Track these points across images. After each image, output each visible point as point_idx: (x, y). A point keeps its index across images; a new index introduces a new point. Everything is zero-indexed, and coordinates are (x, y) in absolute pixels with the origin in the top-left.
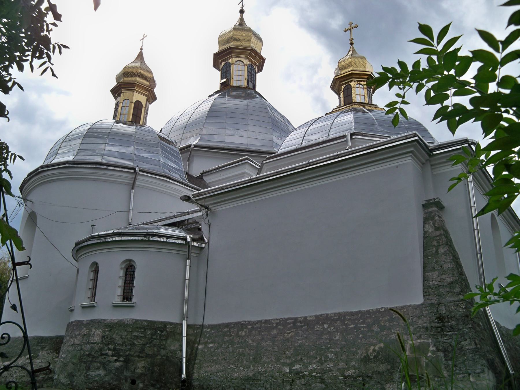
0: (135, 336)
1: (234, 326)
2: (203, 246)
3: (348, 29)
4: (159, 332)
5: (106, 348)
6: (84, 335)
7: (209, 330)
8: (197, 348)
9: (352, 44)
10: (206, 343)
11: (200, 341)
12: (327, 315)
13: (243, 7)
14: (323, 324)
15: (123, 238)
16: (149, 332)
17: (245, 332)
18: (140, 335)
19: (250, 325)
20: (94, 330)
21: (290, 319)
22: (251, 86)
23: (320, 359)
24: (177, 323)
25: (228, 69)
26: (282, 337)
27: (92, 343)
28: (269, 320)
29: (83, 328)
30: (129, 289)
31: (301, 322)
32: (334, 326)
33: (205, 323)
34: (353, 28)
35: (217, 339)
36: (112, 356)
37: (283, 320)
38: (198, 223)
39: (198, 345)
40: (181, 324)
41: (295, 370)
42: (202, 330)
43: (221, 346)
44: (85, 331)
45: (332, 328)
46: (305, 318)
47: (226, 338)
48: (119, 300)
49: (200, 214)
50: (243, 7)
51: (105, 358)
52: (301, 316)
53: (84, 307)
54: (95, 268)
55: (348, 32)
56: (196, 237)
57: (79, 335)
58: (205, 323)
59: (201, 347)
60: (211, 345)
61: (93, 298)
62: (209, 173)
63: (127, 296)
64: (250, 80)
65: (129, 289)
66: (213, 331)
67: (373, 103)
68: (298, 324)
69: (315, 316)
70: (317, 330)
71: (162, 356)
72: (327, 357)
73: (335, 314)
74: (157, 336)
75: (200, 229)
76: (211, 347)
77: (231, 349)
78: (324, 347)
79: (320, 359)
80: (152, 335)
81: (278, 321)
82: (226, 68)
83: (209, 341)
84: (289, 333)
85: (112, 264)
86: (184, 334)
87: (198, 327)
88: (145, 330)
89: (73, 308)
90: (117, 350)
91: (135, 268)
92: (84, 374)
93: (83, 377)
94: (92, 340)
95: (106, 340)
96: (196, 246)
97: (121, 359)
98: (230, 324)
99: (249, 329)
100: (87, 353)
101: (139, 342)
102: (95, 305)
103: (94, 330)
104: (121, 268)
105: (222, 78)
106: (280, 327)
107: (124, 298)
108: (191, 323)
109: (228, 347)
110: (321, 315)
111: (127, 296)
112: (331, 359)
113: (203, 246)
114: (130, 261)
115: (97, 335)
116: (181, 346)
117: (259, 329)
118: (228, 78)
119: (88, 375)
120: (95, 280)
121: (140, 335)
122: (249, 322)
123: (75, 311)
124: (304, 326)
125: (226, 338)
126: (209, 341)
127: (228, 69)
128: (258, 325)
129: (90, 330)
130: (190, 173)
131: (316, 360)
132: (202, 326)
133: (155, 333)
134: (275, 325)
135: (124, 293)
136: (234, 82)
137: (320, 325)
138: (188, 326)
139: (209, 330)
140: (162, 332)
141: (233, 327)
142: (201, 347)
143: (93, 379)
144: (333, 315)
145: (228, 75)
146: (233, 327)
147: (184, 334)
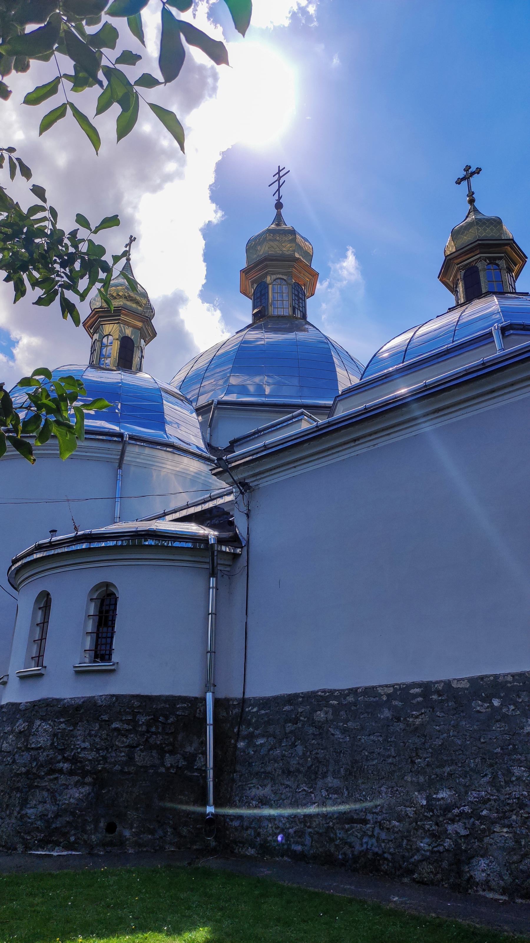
0: (116, 729)
1: (303, 701)
2: (238, 551)
3: (463, 179)
4: (161, 719)
5: (60, 757)
6: (20, 732)
7: (255, 710)
8: (235, 746)
9: (472, 201)
10: (251, 737)
11: (239, 731)
12: (496, 677)
13: (280, 198)
14: (488, 699)
15: (95, 545)
16: (143, 719)
17: (326, 713)
18: (126, 726)
19: (336, 698)
20: (38, 722)
21: (414, 685)
22: (299, 314)
23: (495, 777)
24: (196, 698)
25: (263, 292)
26: (402, 726)
27: (32, 749)
28: (373, 688)
29: (19, 719)
30: (106, 638)
31: (439, 693)
32: (515, 704)
33: (247, 696)
34: (473, 174)
35: (271, 729)
36: (71, 773)
37: (400, 689)
38: (228, 513)
39: (237, 741)
40: (204, 699)
41: (439, 800)
42: (243, 710)
43: (280, 742)
44: (21, 725)
45: (512, 707)
46: (448, 684)
47: (290, 727)
48: (87, 660)
49: (231, 498)
50: (280, 198)
51: (56, 779)
52: (438, 679)
53: (24, 678)
54: (44, 602)
55: (465, 183)
56: (226, 535)
57: (12, 731)
58: (247, 696)
59: (241, 744)
60: (260, 741)
61: (39, 659)
62: (244, 441)
63: (102, 650)
64: (297, 306)
65: (106, 638)
66: (263, 712)
67: (517, 291)
68: (435, 697)
69: (471, 680)
70: (479, 712)
71: (168, 769)
72: (509, 772)
73: (513, 676)
74: (157, 728)
75: (232, 523)
76: (262, 745)
77: (300, 749)
78: (499, 750)
79: (495, 777)
80: (148, 724)
81: (391, 690)
82: (261, 292)
83: (257, 732)
84: (417, 717)
85: (73, 595)
86: (210, 719)
87: (235, 703)
88: (135, 714)
89: (5, 679)
90: (81, 762)
91: (116, 599)
92: (15, 814)
93: (13, 821)
94: (33, 742)
95: (61, 744)
96: (225, 552)
97: (89, 779)
98: (296, 696)
99: (333, 706)
100: (23, 770)
101: (123, 742)
102: (42, 672)
103: (38, 722)
104: (91, 600)
105: (254, 309)
106: (395, 703)
107: (96, 656)
108: (221, 695)
109: (294, 745)
110: (482, 678)
111: (102, 650)
112: (519, 779)
113: (238, 551)
114: (108, 585)
115: (43, 733)
116: (204, 743)
117: (353, 708)
118: (264, 305)
119: (22, 817)
120: (44, 624)
121: (126, 726)
122: (332, 692)
123: (9, 685)
124: (447, 701)
125: (290, 727)
126: (257, 732)
127: (263, 292)
128: (350, 699)
129: (31, 723)
130: (214, 444)
131: (485, 779)
132: (244, 702)
133: (155, 720)
134: (385, 698)
135: (97, 645)
136: (272, 311)
137: (484, 700)
138: (217, 702)
139: (255, 710)
140: (167, 718)
141: (301, 703)
142: (241, 744)
143: (32, 824)
144: (510, 678)
145: (263, 301)
146: (301, 703)
147: (210, 719)
